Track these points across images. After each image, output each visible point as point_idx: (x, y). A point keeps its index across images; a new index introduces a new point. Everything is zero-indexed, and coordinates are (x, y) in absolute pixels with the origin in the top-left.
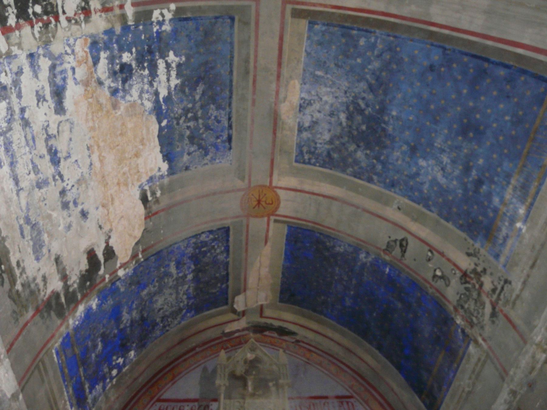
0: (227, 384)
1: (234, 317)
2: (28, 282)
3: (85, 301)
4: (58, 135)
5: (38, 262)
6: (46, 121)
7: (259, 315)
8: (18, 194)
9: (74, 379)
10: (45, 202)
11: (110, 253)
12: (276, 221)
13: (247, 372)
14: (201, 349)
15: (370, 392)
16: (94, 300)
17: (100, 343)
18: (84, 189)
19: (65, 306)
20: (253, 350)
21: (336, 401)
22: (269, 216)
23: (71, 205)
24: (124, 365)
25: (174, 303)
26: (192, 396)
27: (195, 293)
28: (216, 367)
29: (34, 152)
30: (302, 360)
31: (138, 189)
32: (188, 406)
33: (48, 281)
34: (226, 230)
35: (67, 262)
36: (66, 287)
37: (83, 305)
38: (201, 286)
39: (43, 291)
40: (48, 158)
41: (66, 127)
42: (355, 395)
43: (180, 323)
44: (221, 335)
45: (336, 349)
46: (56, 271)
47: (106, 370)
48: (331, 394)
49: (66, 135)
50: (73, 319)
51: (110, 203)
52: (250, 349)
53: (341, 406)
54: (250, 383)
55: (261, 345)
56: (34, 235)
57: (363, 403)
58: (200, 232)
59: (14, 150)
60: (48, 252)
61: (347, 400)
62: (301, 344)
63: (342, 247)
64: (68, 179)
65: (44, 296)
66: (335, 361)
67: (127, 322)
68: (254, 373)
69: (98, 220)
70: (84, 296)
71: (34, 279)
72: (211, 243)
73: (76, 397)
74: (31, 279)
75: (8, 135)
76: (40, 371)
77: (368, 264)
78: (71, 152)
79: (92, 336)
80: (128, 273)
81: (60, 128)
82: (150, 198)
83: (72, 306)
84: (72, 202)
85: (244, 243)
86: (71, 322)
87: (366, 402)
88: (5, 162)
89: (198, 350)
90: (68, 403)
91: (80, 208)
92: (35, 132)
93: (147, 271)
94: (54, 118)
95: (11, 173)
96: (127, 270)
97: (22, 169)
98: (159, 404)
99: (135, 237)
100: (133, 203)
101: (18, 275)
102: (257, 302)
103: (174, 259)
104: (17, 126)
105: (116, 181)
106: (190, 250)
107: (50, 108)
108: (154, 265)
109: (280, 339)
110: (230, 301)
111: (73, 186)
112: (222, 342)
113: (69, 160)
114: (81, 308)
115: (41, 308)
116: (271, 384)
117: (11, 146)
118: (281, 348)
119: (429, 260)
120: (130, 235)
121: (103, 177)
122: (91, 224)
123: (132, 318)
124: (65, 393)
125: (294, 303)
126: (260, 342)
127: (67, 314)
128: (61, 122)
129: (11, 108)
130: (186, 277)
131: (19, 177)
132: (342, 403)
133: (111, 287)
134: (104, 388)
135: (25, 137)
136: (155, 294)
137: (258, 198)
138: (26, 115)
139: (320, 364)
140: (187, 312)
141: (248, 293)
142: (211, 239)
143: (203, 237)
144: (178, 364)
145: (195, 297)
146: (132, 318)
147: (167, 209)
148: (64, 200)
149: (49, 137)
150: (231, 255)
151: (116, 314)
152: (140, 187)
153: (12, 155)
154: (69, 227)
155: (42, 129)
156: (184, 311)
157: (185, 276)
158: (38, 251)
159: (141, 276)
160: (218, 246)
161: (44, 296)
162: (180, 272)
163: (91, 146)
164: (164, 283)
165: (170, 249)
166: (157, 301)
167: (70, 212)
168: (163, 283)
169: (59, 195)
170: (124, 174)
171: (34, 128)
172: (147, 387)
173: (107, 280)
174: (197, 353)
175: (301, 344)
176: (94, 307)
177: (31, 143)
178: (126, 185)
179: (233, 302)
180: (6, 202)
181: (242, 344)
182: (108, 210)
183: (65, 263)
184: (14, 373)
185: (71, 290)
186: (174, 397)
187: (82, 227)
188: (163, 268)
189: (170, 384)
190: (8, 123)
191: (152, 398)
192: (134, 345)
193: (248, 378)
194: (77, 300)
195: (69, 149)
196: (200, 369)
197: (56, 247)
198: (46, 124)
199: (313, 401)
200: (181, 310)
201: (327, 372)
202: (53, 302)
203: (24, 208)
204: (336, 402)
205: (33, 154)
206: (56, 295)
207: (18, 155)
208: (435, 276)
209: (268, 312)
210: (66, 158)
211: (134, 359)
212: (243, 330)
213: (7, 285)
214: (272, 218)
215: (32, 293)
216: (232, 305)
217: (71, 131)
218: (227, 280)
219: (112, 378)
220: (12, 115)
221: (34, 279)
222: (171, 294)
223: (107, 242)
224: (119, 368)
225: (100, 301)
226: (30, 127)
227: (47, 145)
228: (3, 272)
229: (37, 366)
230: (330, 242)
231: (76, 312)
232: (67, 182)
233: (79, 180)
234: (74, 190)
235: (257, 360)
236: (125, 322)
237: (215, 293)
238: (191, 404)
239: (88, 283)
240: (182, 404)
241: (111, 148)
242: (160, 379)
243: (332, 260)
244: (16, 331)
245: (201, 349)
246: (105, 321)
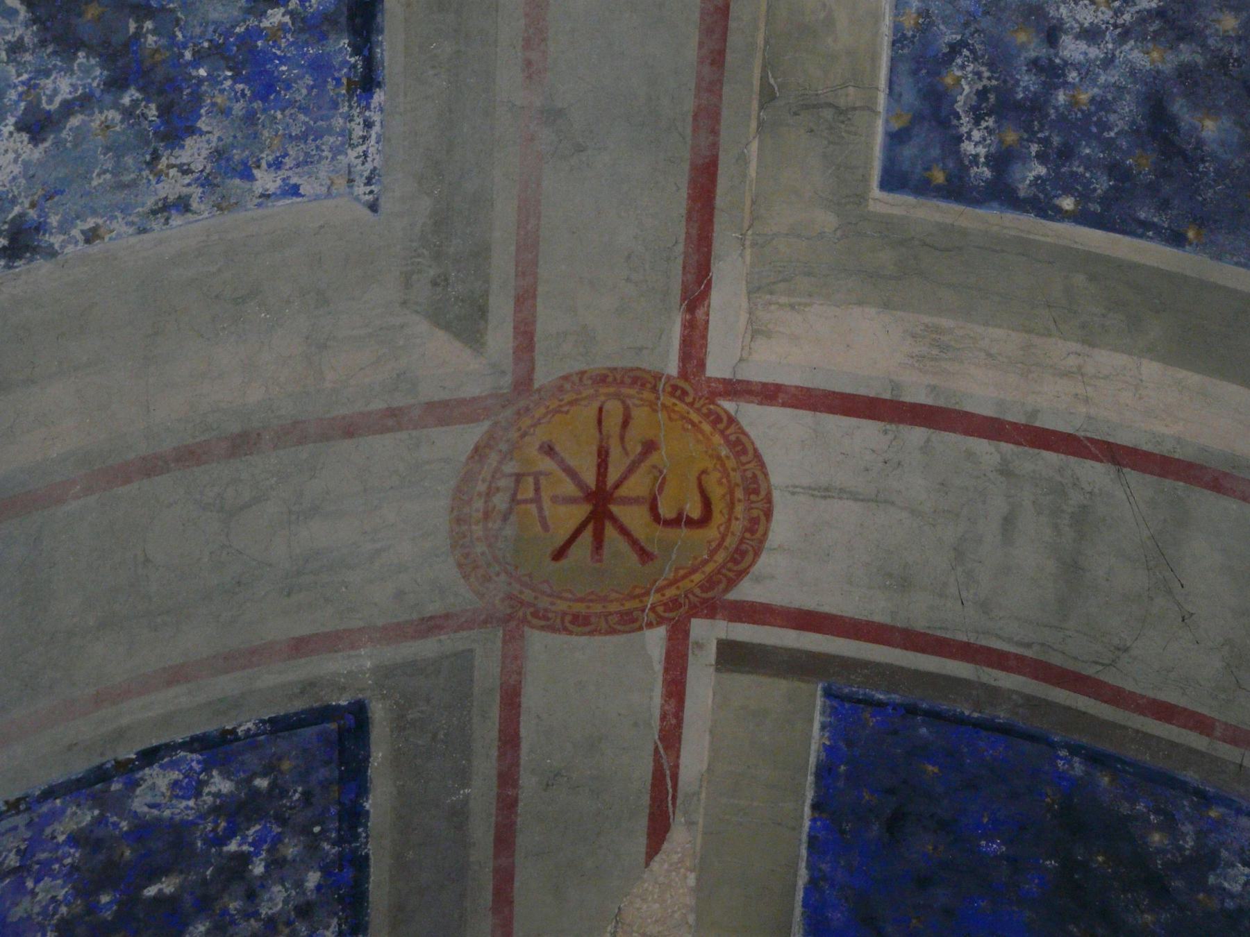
58: (128, 753)
72: (221, 841)
85: (482, 832)
137: (590, 479)
160: (276, 864)
230: (1170, 824)
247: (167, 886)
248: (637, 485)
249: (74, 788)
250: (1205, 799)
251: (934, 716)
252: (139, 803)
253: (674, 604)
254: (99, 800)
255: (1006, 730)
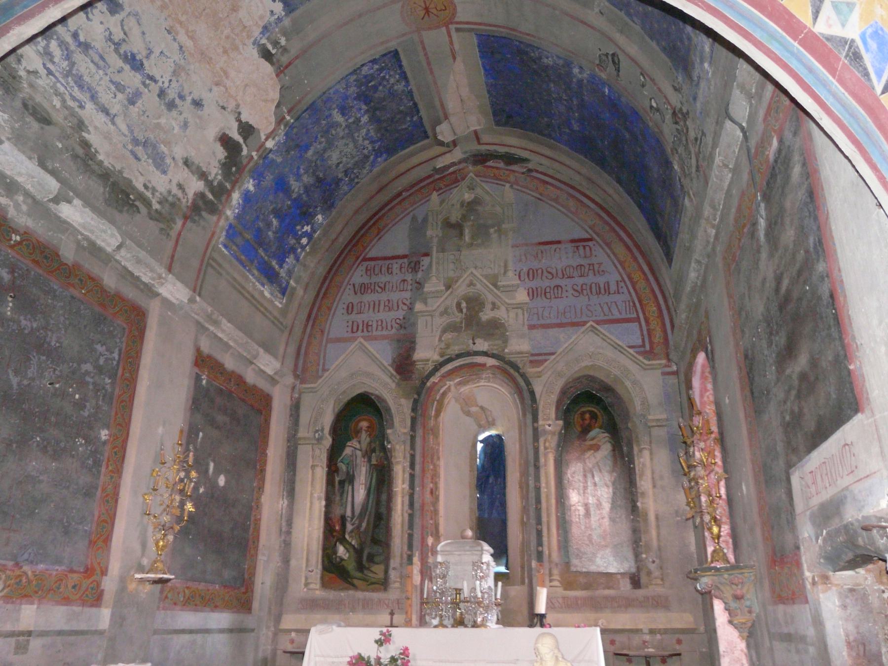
2: (164, 197)
3: (237, 188)
4: (127, 36)
5: (166, 175)
6: (106, 30)
7: (476, 142)
8: (114, 123)
9: (256, 261)
10: (146, 115)
11: (247, 130)
12: (458, 30)
13: (464, 217)
14: (408, 194)
16: (249, 182)
17: (273, 219)
18: (184, 78)
19: (216, 202)
20: (471, 188)
21: (569, 245)
22: (447, 25)
23: (177, 101)
24: (314, 231)
25: (354, 153)
26: (400, 252)
27: (379, 135)
28: (427, 215)
29: (109, 71)
30: (533, 196)
31: (253, 47)
33: (186, 187)
34: (396, 54)
35: (198, 159)
36: (209, 184)
37: (237, 192)
38: (385, 125)
39: (184, 198)
40: (127, 67)
41: (132, 22)
42: (595, 236)
43: (371, 171)
45: (577, 180)
46: (190, 173)
47: (293, 242)
48: (564, 237)
49: (135, 32)
50: (230, 210)
51: (224, 78)
52: (468, 187)
53: (575, 252)
54: (467, 231)
56: (149, 152)
58: (358, 66)
59: (87, 82)
60: (172, 161)
62: (534, 174)
63: (550, 59)
64: (162, 77)
65: (187, 202)
66: (578, 195)
67: (299, 190)
69: (217, 102)
70: (234, 184)
71: (169, 192)
72: (379, 75)
73: (265, 276)
74: (165, 194)
75: (74, 72)
76: (212, 267)
77: (585, 81)
78: (151, 46)
79: (262, 217)
80: (279, 141)
81: (125, 27)
82: (273, 52)
83: (224, 198)
84: (177, 98)
85: (425, 64)
86: (229, 213)
88: (85, 100)
89: (405, 194)
90: (257, 284)
91: (189, 99)
92: (100, 50)
93: (304, 130)
94: (113, 22)
95: (97, 107)
96: (277, 138)
97: (105, 97)
98: (365, 264)
99: (273, 100)
100: (254, 64)
101: (151, 196)
102: (468, 127)
103: (334, 106)
104: (79, 57)
105: (220, 51)
106: (353, 90)
107: (102, 13)
108: (310, 121)
109: (507, 170)
110: (430, 133)
111: (170, 81)
112: (432, 182)
113: (152, 56)
114: (236, 197)
115: (188, 214)
117: (83, 80)
118: (509, 182)
119: (643, 86)
120: (266, 101)
121: (202, 54)
122: (210, 109)
124: (250, 277)
125: (514, 126)
126: (480, 176)
127: (220, 207)
128: (123, 20)
129: (62, 42)
130: (360, 121)
131: (106, 106)
132: (577, 247)
133: (264, 162)
135: (92, 61)
136: (325, 150)
137: (423, 5)
138: (82, 39)
139: (556, 200)
140: (376, 157)
141: (453, 119)
142: (378, 70)
143: (365, 70)
144: (384, 215)
145: (380, 140)
147: (304, 52)
148: (167, 101)
149: (117, 45)
150: (412, 82)
151: (281, 185)
152: (254, 44)
153: (88, 88)
154: (185, 125)
155: (106, 42)
156: (372, 157)
157: (358, 120)
158: (161, 165)
159: (298, 139)
160: (390, 76)
161: (187, 202)
162: (349, 118)
163: (171, 27)
164: (332, 135)
165: (324, 98)
166: (330, 157)
167: (180, 109)
169: (158, 99)
170: (227, 37)
171: (97, 47)
173: (256, 158)
174: (404, 199)
175: (534, 174)
176: (251, 188)
177: (101, 63)
178: (236, 48)
180: (105, 138)
181: (459, 181)
182: (225, 86)
183: (196, 162)
184: (182, 282)
185: (215, 184)
186: (380, 255)
187: (200, 118)
188: (324, 120)
189: (375, 240)
190: (68, 60)
191: (357, 258)
192: (319, 209)
193: (465, 224)
194: (228, 190)
195: (146, 44)
196: (408, 219)
197: (179, 152)
198: (107, 33)
199: (542, 247)
200: (367, 157)
201: (563, 210)
202: (200, 203)
203: (127, 133)
204: (569, 246)
205: (109, 73)
206: (201, 196)
207: (94, 85)
208: (651, 107)
209: (485, 138)
210: (148, 57)
211: (325, 223)
212: (460, 162)
213: (143, 210)
214: (452, 27)
215: (173, 205)
216: (436, 137)
217: (140, 25)
218: (418, 111)
219: (303, 247)
220: (67, 49)
221: (169, 192)
223: (239, 120)
224: (310, 236)
225: (256, 181)
226: (92, 48)
227: (120, 55)
228: (134, 201)
229: (208, 264)
230: (534, 52)
231: (231, 201)
232: (161, 80)
233: (174, 71)
234: (174, 84)
235: (476, 201)
236: (296, 190)
237: (406, 129)
238: (400, 261)
239: (234, 169)
240: (391, 261)
241: (197, 17)
243: (544, 74)
244: (171, 244)
246: (271, 197)
247: (373, 83)
248: (432, 6)
249: (351, 74)
250: (538, 48)
251: (493, 36)
252: (363, 73)
253: (445, 23)
254: (356, 74)
255: (505, 38)
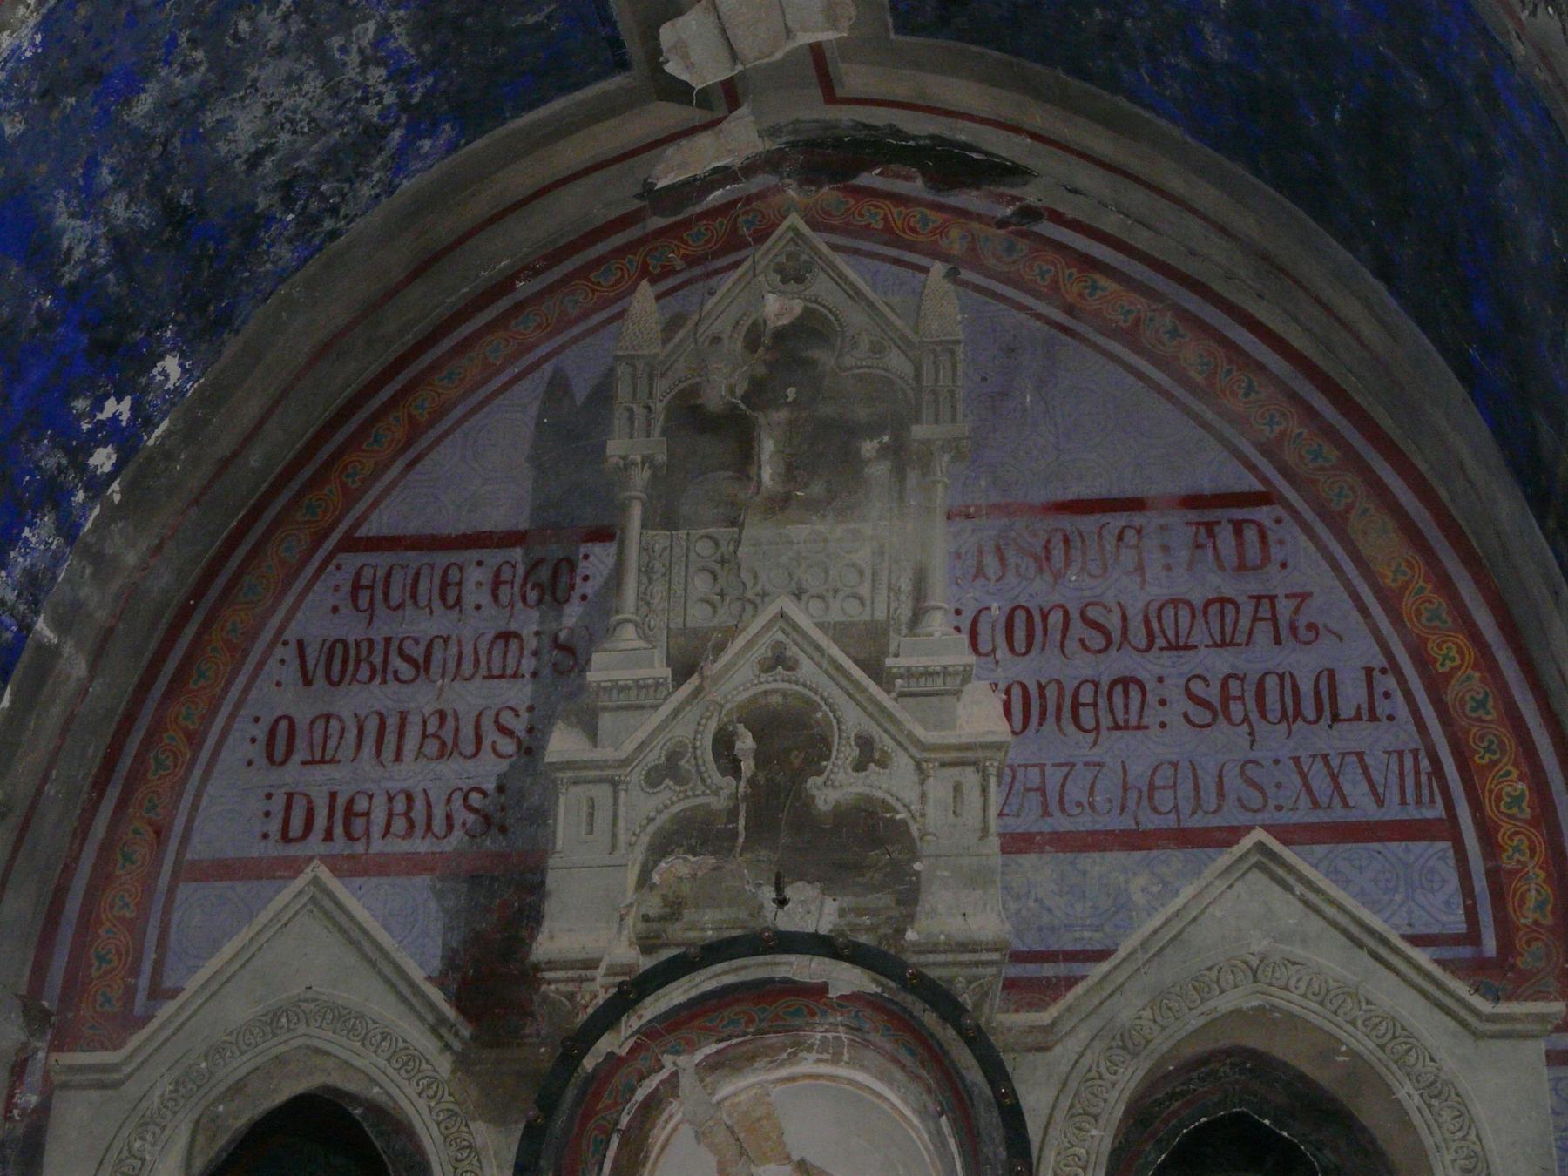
0: (662, 458)
1: (697, 115)
7: (817, 93)
13: (760, 392)
14: (537, 284)
15: (1366, 471)
20: (793, 275)
21: (1177, 519)
24: (144, 418)
25: (324, 113)
26: (497, 519)
30: (1039, 317)
32: (480, 563)
43: (390, 189)
44: (637, 204)
52: (780, 270)
53: (1199, 546)
54: (768, 447)
55: (835, 248)
57: (1320, 528)
61: (1239, 514)
62: (1047, 228)
67: (91, 251)
68: (791, 392)
87: (1337, 523)
98: (351, 562)
109: (940, 207)
110: (634, 49)
116: (868, 447)
118: (937, 255)
123: (112, 229)
126: (831, 229)
132: (1210, 527)
134: (69, 530)
136: (204, 97)
139: (1130, 336)
140: (414, 133)
144: (434, 367)
146: (112, 229)
159: (98, 44)
164: (236, 37)
166: (225, 125)
168: (229, 42)
172: (295, 485)
174: (519, 307)
175: (1047, 228)
179: (655, 55)
186: (413, 527)
196: (530, 393)
199: (1068, 522)
209: (856, 78)
212: (750, 168)
219: (96, 486)
222: (294, 79)
224: (124, 439)
236: (80, 252)
238: (494, 557)
242: (353, 442)
245: (537, 284)
